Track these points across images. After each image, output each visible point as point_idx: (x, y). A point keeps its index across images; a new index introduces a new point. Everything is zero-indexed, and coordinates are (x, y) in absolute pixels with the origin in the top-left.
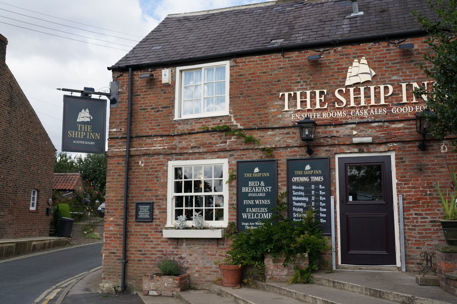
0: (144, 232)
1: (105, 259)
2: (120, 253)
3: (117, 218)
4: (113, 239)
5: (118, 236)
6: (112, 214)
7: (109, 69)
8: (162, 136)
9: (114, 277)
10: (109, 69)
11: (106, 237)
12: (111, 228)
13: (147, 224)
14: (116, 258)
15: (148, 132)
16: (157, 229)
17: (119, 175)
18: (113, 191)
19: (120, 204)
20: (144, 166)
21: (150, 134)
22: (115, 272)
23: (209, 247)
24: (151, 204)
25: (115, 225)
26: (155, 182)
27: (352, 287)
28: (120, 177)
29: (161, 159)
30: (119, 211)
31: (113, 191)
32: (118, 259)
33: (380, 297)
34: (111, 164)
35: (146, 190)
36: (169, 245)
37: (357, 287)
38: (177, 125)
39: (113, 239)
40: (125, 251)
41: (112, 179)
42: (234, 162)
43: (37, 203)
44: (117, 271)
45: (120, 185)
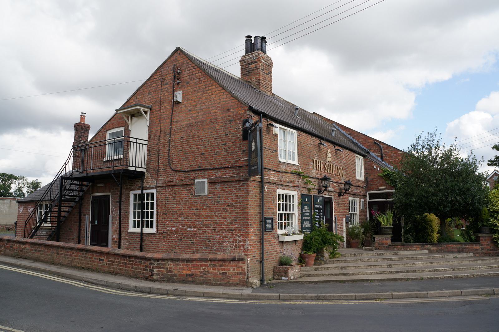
0: (269, 239)
1: (250, 262)
2: (258, 257)
3: (255, 230)
4: (254, 246)
5: (257, 243)
6: (253, 226)
7: (83, 117)
8: (274, 171)
9: (255, 274)
10: (83, 117)
11: (250, 245)
12: (252, 238)
13: (270, 233)
14: (256, 260)
15: (268, 166)
16: (274, 236)
17: (256, 196)
18: (253, 208)
19: (256, 219)
20: (267, 191)
21: (269, 168)
22: (255, 271)
23: (293, 245)
24: (272, 219)
25: (255, 235)
26: (273, 203)
27: (367, 254)
28: (256, 197)
29: (275, 187)
30: (256, 224)
31: (253, 208)
32: (257, 261)
33: (383, 255)
34: (251, 186)
35: (269, 209)
36: (279, 246)
37: (370, 254)
38: (280, 165)
39: (254, 246)
40: (262, 254)
41: (252, 198)
42: (300, 194)
43: (157, 222)
44: (257, 270)
45: (256, 203)
